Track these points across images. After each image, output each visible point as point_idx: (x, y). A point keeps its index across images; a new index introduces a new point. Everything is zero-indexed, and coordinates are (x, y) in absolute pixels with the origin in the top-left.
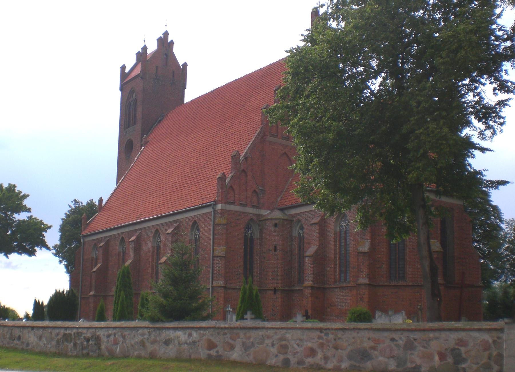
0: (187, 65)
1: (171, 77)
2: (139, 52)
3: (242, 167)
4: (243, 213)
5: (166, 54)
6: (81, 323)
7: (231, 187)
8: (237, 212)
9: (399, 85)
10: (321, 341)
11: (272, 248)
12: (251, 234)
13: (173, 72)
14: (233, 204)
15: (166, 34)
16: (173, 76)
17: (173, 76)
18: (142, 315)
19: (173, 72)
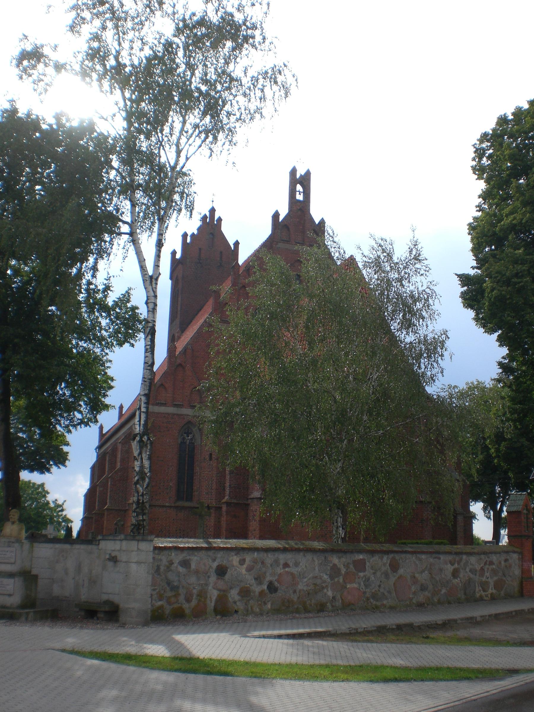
0: (239, 243)
1: (219, 259)
2: (193, 233)
3: (179, 361)
4: (178, 415)
5: (212, 234)
6: (459, 546)
7: (162, 385)
8: (168, 414)
9: (8, 260)
10: (472, 576)
11: (207, 457)
12: (191, 439)
13: (221, 252)
14: (164, 405)
15: (212, 211)
16: (221, 258)
17: (221, 258)
18: (165, 535)
19: (221, 252)
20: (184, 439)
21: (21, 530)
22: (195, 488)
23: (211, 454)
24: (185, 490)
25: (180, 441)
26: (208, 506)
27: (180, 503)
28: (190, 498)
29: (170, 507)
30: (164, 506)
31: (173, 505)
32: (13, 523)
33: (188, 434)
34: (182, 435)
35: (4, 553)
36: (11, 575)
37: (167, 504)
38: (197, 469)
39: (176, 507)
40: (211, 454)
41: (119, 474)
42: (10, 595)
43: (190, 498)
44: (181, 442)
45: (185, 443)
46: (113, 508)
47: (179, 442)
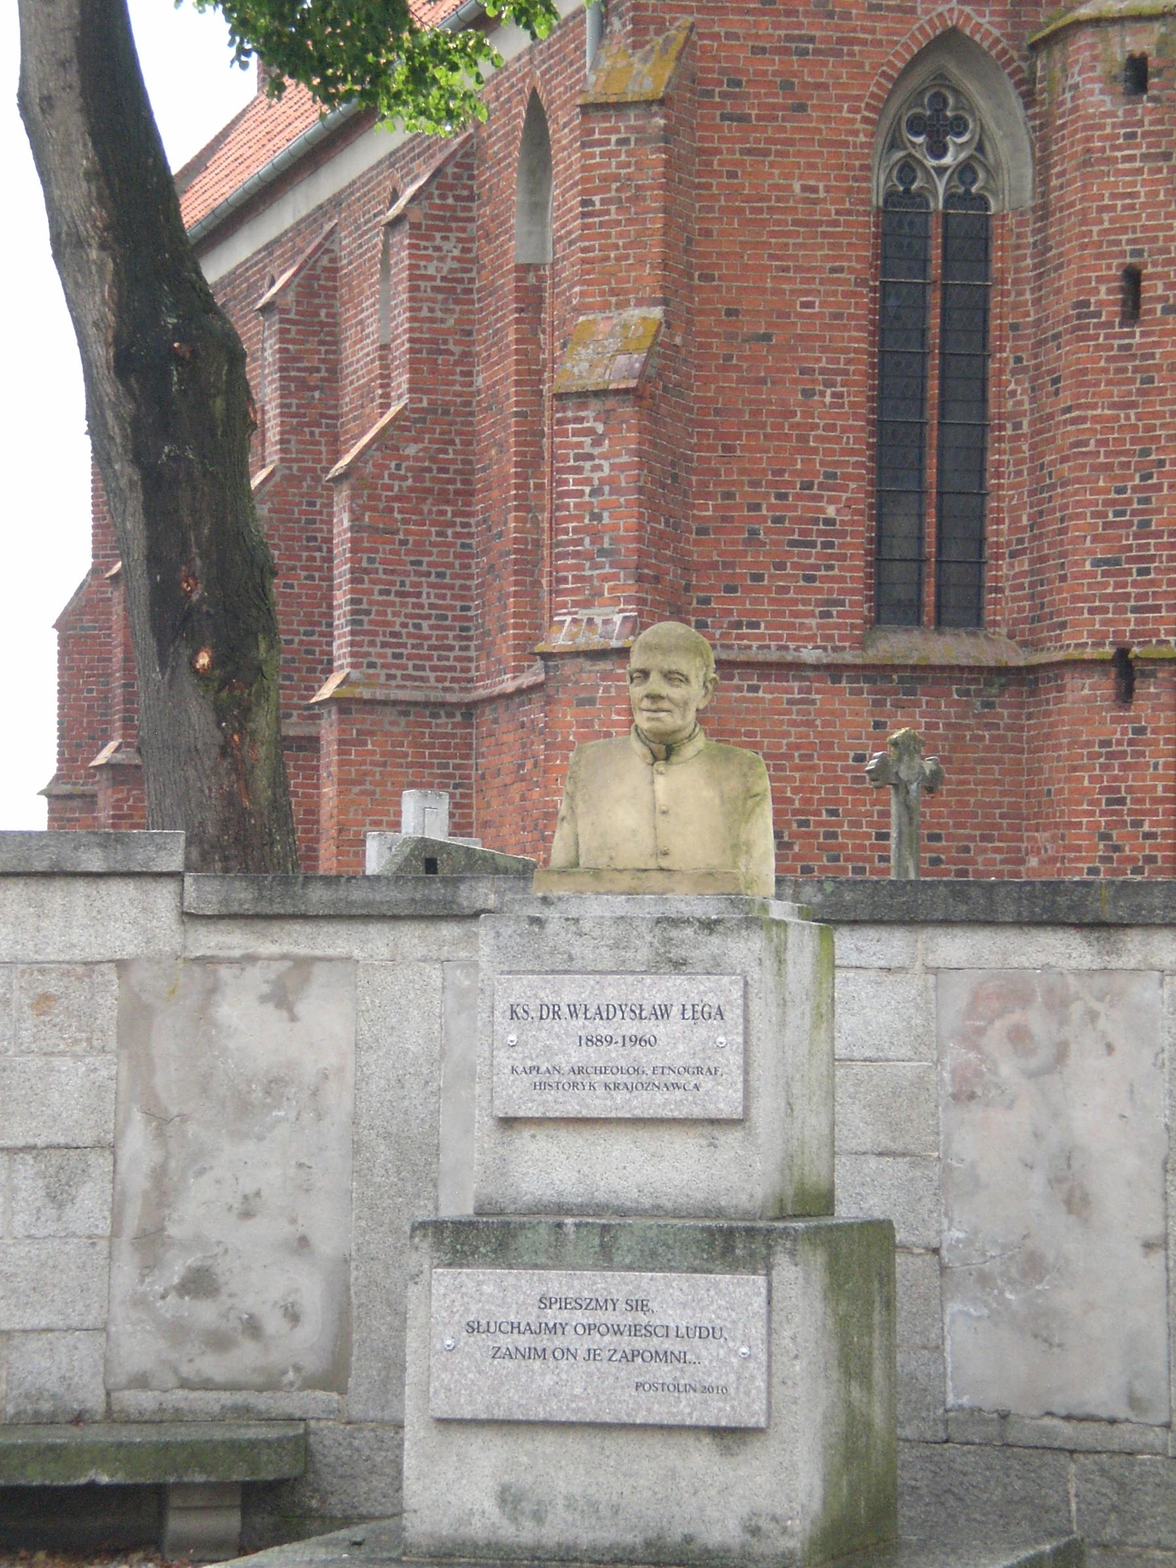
11: (1106, 296)
12: (965, 171)
20: (907, 169)
21: (738, 810)
22: (998, 532)
23: (1133, 278)
24: (930, 549)
25: (879, 184)
26: (1122, 653)
27: (899, 645)
28: (964, 608)
29: (834, 671)
30: (798, 667)
31: (849, 657)
32: (664, 749)
33: (937, 132)
34: (894, 144)
35: (632, 1028)
36: (727, 1241)
37: (809, 655)
38: (1011, 393)
39: (875, 673)
40: (1133, 278)
41: (411, 450)
42: (730, 1436)
43: (964, 608)
44: (890, 196)
45: (919, 200)
46: (380, 694)
47: (877, 199)
